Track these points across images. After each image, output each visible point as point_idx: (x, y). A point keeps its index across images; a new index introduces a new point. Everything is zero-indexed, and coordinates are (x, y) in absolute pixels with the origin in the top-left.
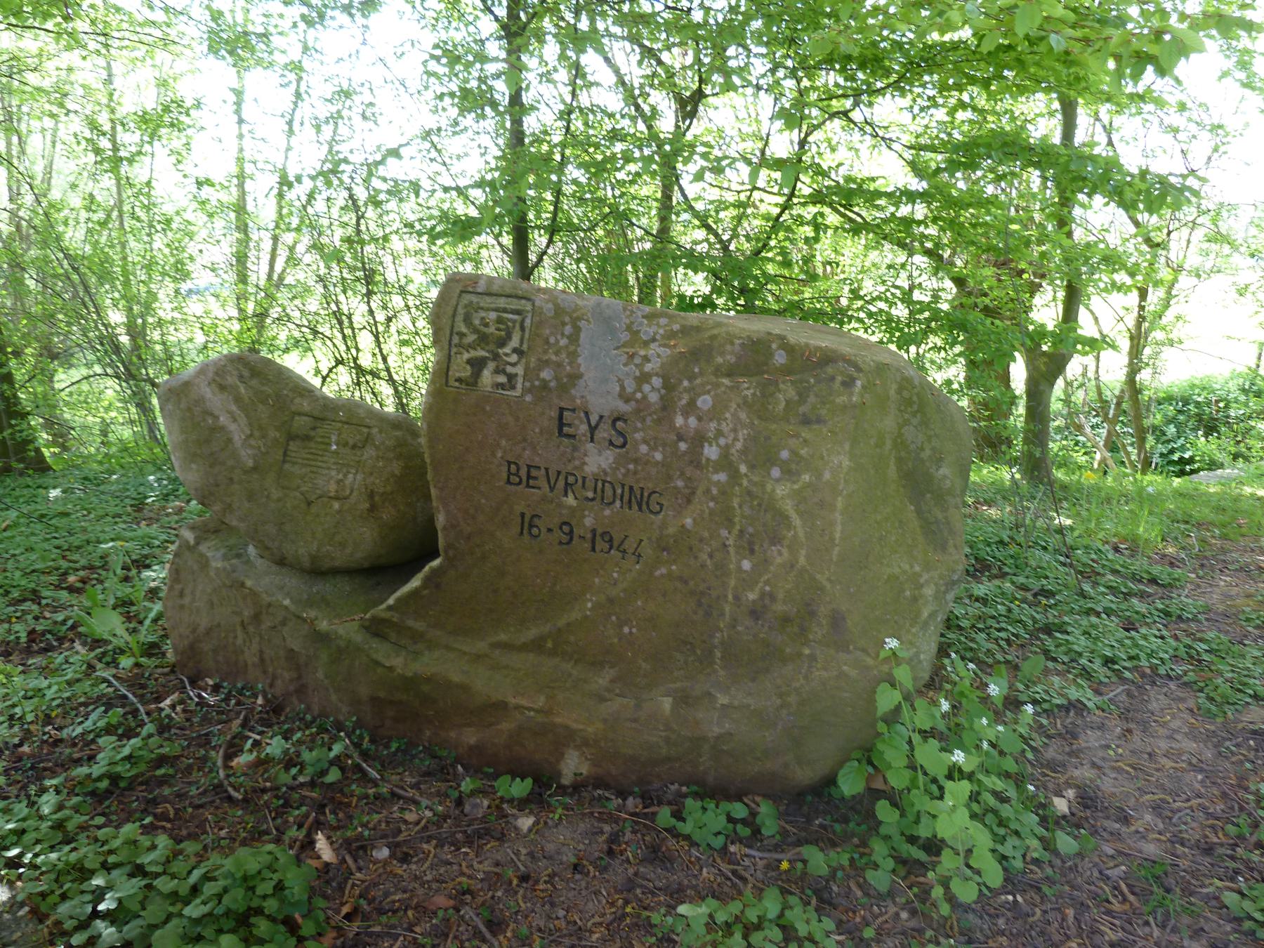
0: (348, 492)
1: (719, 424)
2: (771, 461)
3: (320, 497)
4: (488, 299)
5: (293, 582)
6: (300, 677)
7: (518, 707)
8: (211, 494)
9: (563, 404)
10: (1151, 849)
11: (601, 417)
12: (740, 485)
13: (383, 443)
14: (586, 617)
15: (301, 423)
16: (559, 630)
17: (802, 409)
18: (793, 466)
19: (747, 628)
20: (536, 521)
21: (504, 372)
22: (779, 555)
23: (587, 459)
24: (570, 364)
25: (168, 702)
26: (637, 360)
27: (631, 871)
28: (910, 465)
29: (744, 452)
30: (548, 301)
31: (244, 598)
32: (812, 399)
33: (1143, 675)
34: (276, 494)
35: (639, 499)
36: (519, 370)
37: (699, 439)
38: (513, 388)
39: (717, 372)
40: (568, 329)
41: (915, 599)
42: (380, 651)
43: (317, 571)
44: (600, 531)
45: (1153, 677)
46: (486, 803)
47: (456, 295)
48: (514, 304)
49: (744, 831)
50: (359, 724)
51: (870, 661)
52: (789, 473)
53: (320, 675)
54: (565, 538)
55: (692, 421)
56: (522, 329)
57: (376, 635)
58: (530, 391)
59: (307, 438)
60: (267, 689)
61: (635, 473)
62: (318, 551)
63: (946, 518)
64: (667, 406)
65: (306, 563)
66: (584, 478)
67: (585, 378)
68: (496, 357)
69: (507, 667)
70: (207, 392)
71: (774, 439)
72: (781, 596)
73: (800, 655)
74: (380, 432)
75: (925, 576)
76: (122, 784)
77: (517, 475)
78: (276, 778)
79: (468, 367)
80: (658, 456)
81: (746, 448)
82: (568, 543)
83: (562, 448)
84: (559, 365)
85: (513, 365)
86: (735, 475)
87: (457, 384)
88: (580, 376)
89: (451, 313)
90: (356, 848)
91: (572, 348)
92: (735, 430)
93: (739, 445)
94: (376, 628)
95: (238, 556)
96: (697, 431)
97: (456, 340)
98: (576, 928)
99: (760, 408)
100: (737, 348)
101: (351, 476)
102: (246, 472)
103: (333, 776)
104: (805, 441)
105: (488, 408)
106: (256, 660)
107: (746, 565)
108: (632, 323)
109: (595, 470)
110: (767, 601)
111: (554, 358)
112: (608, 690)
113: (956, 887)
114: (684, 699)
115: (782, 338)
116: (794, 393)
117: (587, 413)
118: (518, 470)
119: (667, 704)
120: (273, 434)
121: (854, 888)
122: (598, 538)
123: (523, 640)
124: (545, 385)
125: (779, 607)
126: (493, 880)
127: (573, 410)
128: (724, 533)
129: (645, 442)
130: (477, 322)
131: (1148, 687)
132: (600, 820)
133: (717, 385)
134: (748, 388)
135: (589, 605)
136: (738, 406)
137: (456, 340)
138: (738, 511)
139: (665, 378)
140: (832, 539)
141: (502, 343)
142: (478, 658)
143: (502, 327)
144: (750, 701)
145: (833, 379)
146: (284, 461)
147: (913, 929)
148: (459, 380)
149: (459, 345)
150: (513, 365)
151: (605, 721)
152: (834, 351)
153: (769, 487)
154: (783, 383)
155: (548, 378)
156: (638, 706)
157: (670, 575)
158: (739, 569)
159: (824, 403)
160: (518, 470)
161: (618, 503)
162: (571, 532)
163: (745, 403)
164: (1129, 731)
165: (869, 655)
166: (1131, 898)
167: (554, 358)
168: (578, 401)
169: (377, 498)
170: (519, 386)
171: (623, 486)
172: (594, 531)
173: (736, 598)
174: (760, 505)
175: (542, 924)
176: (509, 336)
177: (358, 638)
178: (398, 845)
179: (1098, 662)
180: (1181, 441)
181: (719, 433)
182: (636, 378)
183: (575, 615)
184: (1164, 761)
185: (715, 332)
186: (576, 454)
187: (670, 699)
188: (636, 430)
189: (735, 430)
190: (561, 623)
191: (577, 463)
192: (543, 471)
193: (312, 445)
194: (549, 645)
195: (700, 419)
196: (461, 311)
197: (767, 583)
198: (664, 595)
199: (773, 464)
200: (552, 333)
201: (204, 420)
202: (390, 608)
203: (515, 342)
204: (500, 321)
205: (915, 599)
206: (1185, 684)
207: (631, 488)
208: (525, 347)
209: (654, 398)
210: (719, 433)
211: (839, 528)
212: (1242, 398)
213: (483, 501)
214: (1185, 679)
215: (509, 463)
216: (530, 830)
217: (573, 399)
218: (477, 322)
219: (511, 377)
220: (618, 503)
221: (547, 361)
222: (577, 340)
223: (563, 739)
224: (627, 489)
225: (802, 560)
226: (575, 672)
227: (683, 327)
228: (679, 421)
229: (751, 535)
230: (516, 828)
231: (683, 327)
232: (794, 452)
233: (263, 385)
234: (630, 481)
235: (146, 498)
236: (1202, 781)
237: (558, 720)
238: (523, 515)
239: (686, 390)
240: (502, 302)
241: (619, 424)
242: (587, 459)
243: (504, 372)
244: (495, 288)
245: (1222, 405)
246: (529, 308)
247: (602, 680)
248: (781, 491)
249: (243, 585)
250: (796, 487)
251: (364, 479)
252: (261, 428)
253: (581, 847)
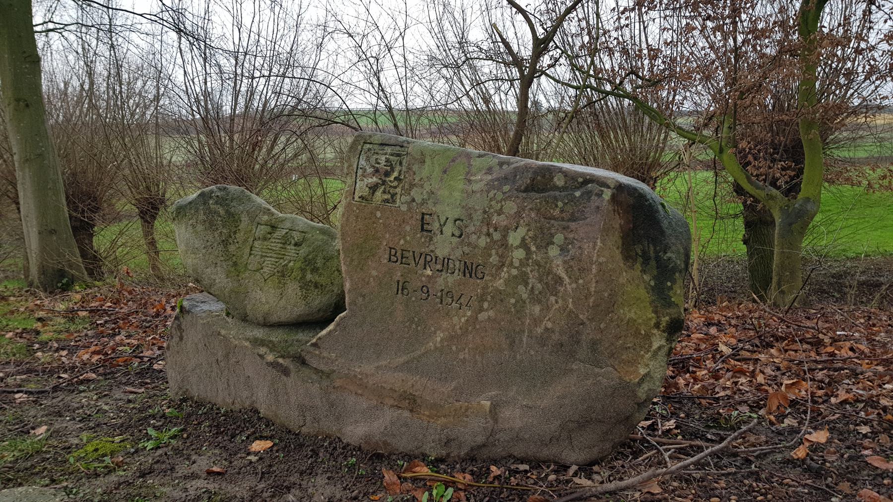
68: (384, 183)
77: (395, 255)
150: (395, 187)
173: (530, 331)
176: (393, 170)
192: (411, 253)
203: (396, 174)
225: (570, 306)
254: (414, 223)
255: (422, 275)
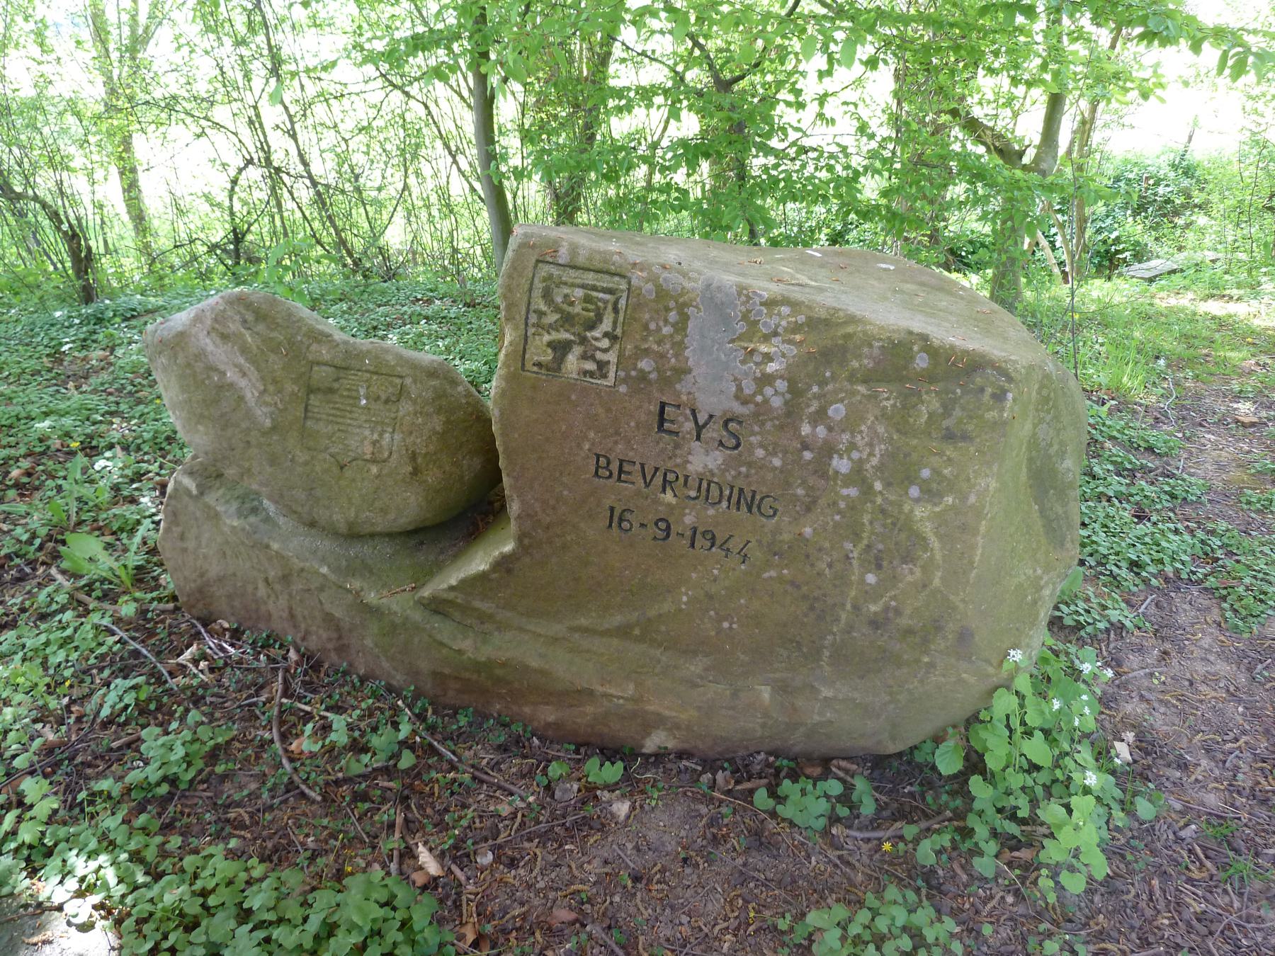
0: (386, 455)
1: (853, 436)
2: (910, 479)
3: (355, 459)
4: (572, 273)
5: (325, 545)
6: (340, 638)
7: (605, 695)
8: (224, 458)
9: (664, 399)
10: (1213, 800)
11: (711, 416)
12: (873, 502)
13: (420, 396)
14: (681, 610)
15: (321, 375)
16: (649, 620)
17: (945, 423)
18: (934, 486)
19: (864, 635)
20: (627, 515)
21: (593, 358)
22: (910, 574)
23: (690, 458)
24: (676, 356)
25: (188, 654)
26: (757, 358)
27: (740, 861)
28: (1038, 463)
29: (880, 468)
30: (648, 281)
31: (270, 559)
32: (958, 412)
33: (1167, 580)
34: (302, 457)
35: (747, 501)
36: (612, 357)
37: (828, 450)
38: (605, 376)
39: (852, 378)
40: (673, 316)
41: (1035, 602)
42: (443, 630)
43: (354, 535)
44: (700, 529)
45: (1175, 582)
46: (576, 787)
47: (530, 269)
48: (606, 282)
49: (843, 812)
50: (417, 695)
51: (991, 670)
52: (930, 494)
53: (369, 642)
54: (661, 534)
55: (821, 431)
56: (616, 310)
57: (436, 612)
58: (624, 381)
59: (331, 391)
60: (299, 641)
61: (747, 476)
62: (357, 517)
63: (1065, 512)
64: (792, 413)
65: (343, 528)
66: (687, 477)
67: (694, 373)
68: (583, 341)
69: (588, 651)
70: (208, 344)
71: (915, 456)
72: (908, 611)
73: (918, 661)
74: (415, 382)
75: (1046, 578)
76: (183, 786)
77: (607, 468)
78: (348, 768)
79: (549, 351)
80: (777, 462)
81: (882, 464)
82: (664, 539)
83: (661, 445)
84: (662, 356)
85: (605, 351)
86: (867, 491)
87: (535, 369)
88: (689, 371)
89: (526, 287)
90: (458, 855)
91: (678, 338)
92: (871, 445)
93: (875, 461)
94: (437, 607)
95: (254, 511)
96: (826, 441)
97: (533, 319)
98: (702, 935)
99: (900, 421)
100: (876, 352)
101: (387, 435)
102: (264, 434)
103: (407, 760)
104: (949, 459)
105: (573, 397)
106: (285, 615)
107: (871, 578)
108: (749, 311)
109: (700, 470)
110: (891, 615)
111: (655, 347)
112: (701, 678)
113: (1065, 878)
114: (783, 688)
115: (924, 338)
116: (938, 405)
117: (694, 412)
118: (608, 463)
119: (766, 693)
120: (290, 387)
121: (959, 871)
122: (698, 536)
123: (607, 626)
124: (643, 376)
125: (904, 622)
126: (607, 881)
127: (678, 407)
128: (849, 546)
129: (761, 446)
130: (559, 299)
131: (1173, 594)
132: (694, 799)
133: (854, 393)
134: (888, 398)
135: (685, 599)
136: (876, 418)
137: (533, 319)
138: (868, 527)
139: (792, 383)
140: (971, 563)
141: (592, 326)
142: (555, 640)
143: (592, 307)
144: (856, 695)
145: (982, 390)
146: (306, 418)
147: (1021, 916)
148: (539, 365)
149: (537, 325)
150: (605, 351)
151: (699, 708)
152: (983, 356)
153: (906, 508)
154: (927, 393)
155: (647, 369)
156: (735, 694)
157: (780, 579)
158: (862, 581)
159: (971, 418)
160: (608, 463)
161: (724, 504)
162: (668, 527)
163: (884, 416)
164: (1165, 653)
165: (991, 665)
166: (1208, 864)
167: (655, 347)
168: (684, 398)
169: (419, 460)
170: (612, 375)
171: (732, 488)
172: (695, 530)
173: (856, 608)
174: (894, 524)
175: (668, 933)
176: (599, 318)
177: (417, 616)
178: (500, 847)
179: (1124, 564)
180: (1109, 221)
181: (852, 446)
182: (755, 379)
183: (667, 607)
184: (1203, 688)
185: (850, 329)
186: (678, 452)
187: (769, 688)
188: (753, 434)
189: (871, 445)
190: (652, 613)
191: (679, 460)
192: (638, 467)
193: (336, 398)
194: (637, 632)
195: (830, 429)
196: (539, 285)
197: (894, 598)
198: (772, 596)
199: (912, 483)
200: (652, 319)
201: (209, 377)
202: (452, 588)
203: (606, 325)
204: (587, 299)
205: (1035, 602)
206: (1206, 589)
207: (741, 490)
208: (619, 332)
209: (777, 402)
210: (852, 446)
211: (979, 552)
212: (1172, 175)
213: (565, 493)
214: (1207, 584)
215: (598, 456)
216: (628, 817)
217: (678, 394)
218: (559, 299)
219: (602, 365)
220: (724, 504)
221: (646, 350)
222: (685, 329)
223: (651, 723)
224: (736, 491)
225: (937, 582)
226: (664, 659)
227: (810, 319)
228: (806, 429)
229: (880, 551)
230: (613, 815)
231: (810, 319)
232: (936, 472)
233: (272, 330)
234: (740, 483)
235: (61, 344)
236: (1243, 714)
237: (651, 708)
238: (612, 509)
239: (817, 397)
240: (590, 278)
241: (732, 426)
242: (690, 458)
243: (593, 358)
244: (581, 260)
245: (1151, 182)
246: (624, 286)
247: (695, 667)
248: (920, 512)
249: (268, 547)
250: (937, 509)
251: (404, 440)
252: (275, 382)
253: (683, 833)
254: (643, 418)
255: (656, 502)
